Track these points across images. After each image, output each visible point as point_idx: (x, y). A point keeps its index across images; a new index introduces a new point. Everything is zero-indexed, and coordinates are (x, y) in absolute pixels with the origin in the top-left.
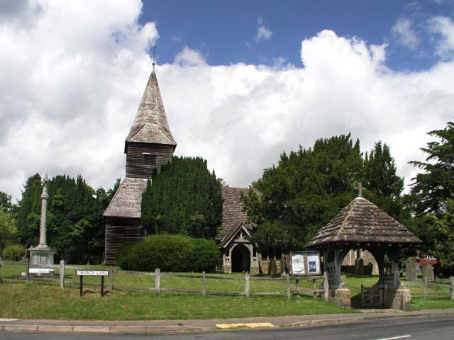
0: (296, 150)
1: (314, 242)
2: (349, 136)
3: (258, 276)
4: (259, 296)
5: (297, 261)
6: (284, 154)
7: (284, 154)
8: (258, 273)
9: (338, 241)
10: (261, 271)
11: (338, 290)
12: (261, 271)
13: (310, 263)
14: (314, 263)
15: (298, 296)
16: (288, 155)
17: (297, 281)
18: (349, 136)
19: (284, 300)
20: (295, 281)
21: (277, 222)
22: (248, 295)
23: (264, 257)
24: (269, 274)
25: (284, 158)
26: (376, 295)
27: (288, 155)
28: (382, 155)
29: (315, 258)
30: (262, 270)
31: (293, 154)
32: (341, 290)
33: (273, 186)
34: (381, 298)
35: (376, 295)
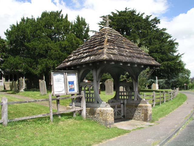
0: (30, 17)
1: (69, 64)
2: (61, 11)
3: (3, 91)
4: (19, 121)
5: (59, 81)
6: (24, 18)
7: (24, 18)
8: (3, 89)
9: (106, 60)
10: (5, 89)
11: (99, 109)
12: (5, 89)
13: (70, 83)
14: (72, 83)
15: (60, 117)
16: (25, 19)
17: (58, 101)
18: (61, 11)
19: (48, 123)
20: (55, 101)
21: (18, 57)
22: (6, 123)
23: (7, 80)
24: (11, 90)
25: (23, 20)
26: (119, 109)
27: (25, 19)
28: (81, 23)
29: (73, 78)
30: (6, 87)
31: (28, 19)
32: (102, 109)
33: (17, 33)
34: (122, 111)
35: (119, 109)
